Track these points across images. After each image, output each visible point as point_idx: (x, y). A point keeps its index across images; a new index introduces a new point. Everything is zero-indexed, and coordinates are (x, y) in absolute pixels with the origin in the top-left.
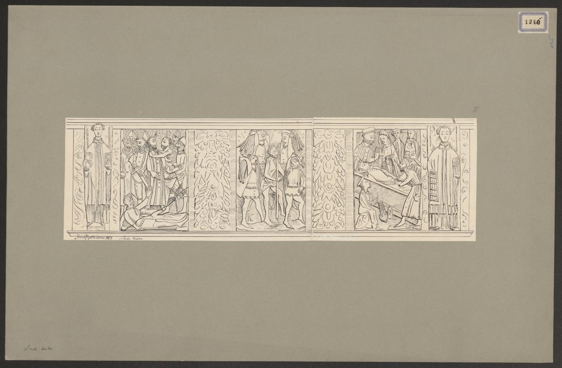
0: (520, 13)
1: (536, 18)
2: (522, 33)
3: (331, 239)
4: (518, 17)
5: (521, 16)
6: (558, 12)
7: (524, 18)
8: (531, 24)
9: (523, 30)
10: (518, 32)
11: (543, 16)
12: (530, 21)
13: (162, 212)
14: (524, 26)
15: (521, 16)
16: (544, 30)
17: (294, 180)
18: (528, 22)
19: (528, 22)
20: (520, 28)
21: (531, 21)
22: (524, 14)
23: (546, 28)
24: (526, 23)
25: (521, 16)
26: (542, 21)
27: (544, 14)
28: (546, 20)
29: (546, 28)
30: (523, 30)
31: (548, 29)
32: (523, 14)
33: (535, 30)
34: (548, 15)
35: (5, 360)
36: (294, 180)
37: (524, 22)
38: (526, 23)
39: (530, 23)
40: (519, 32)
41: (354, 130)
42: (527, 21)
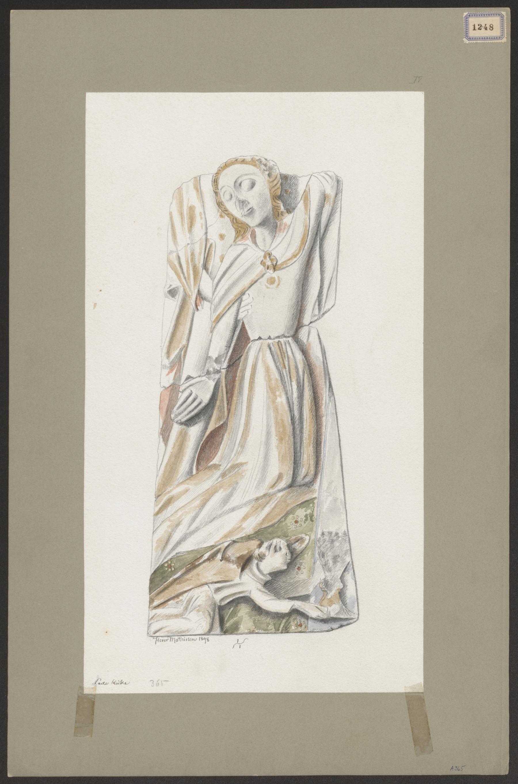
0: (465, 14)
3: (234, 591)
5: (467, 18)
6: (511, 12)
7: (472, 21)
8: (481, 29)
9: (470, 39)
10: (505, 42)
12: (479, 25)
14: (472, 33)
16: (500, 38)
17: (345, 532)
18: (477, 27)
19: (477, 27)
20: (467, 36)
21: (480, 26)
22: (471, 16)
23: (502, 35)
24: (474, 29)
25: (467, 18)
27: (499, 15)
30: (470, 39)
31: (506, 36)
32: (469, 15)
33: (494, 38)
36: (345, 532)
37: (471, 28)
38: (474, 29)
39: (479, 29)
40: (466, 41)
41: (249, 310)
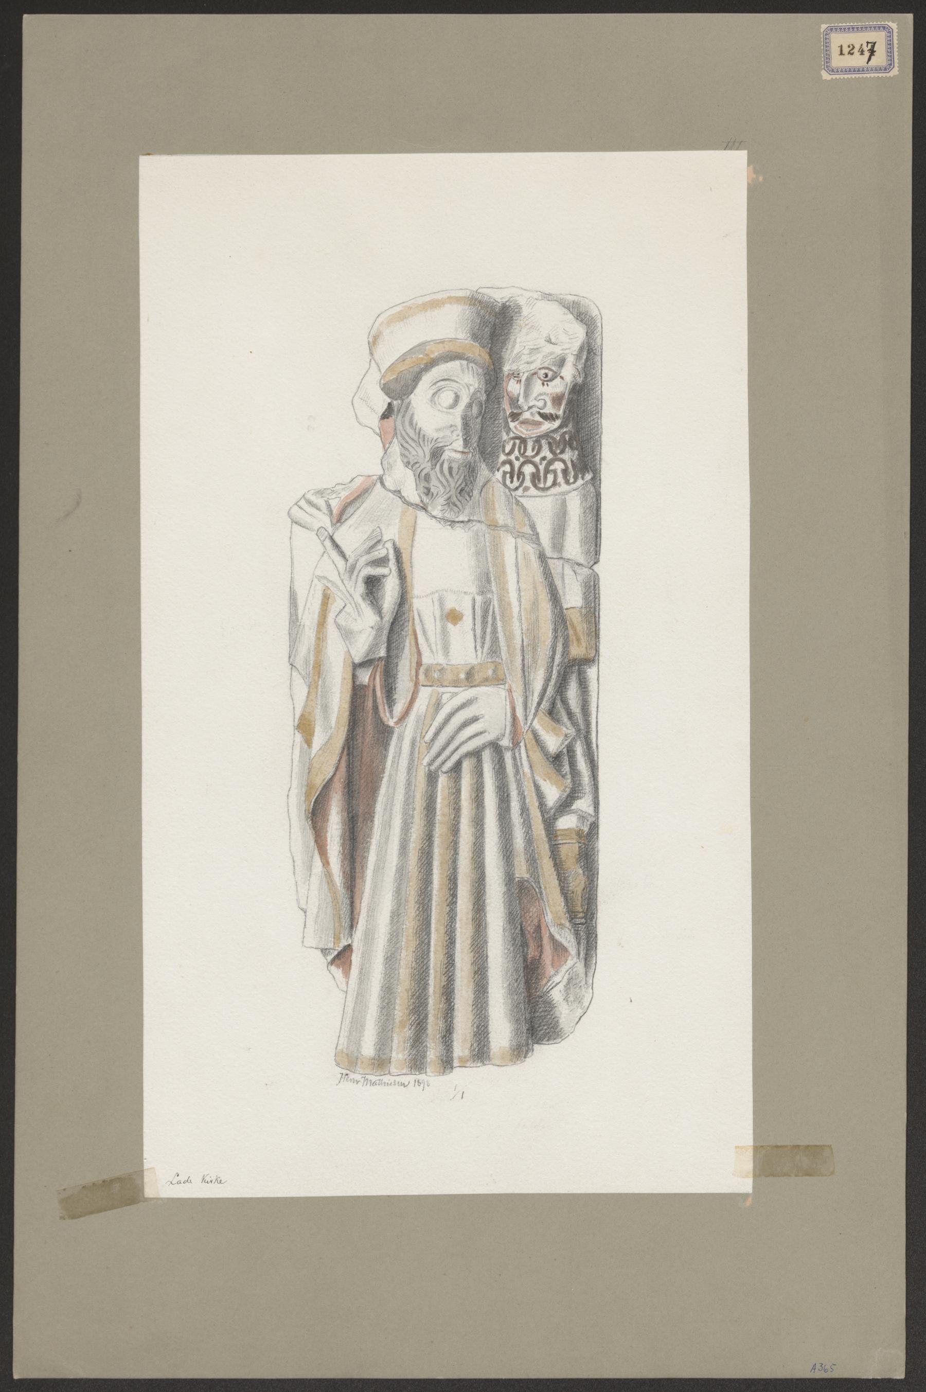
0: (824, 26)
1: (859, 39)
2: (896, 65)
4: (840, 22)
7: (838, 40)
8: (852, 54)
11: (883, 34)
12: (849, 47)
13: (413, 439)
14: (837, 61)
15: (827, 37)
19: (846, 50)
21: (851, 47)
23: (891, 64)
24: (841, 54)
26: (881, 49)
27: (884, 28)
28: (890, 45)
29: (891, 64)
30: (833, 71)
33: (850, 71)
34: (895, 31)
35: (14, 1380)
37: (835, 51)
38: (841, 54)
39: (850, 53)
40: (825, 76)
42: (841, 46)
